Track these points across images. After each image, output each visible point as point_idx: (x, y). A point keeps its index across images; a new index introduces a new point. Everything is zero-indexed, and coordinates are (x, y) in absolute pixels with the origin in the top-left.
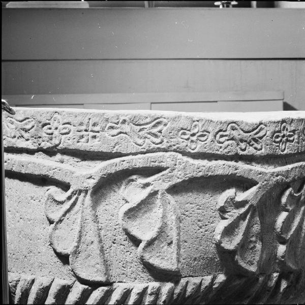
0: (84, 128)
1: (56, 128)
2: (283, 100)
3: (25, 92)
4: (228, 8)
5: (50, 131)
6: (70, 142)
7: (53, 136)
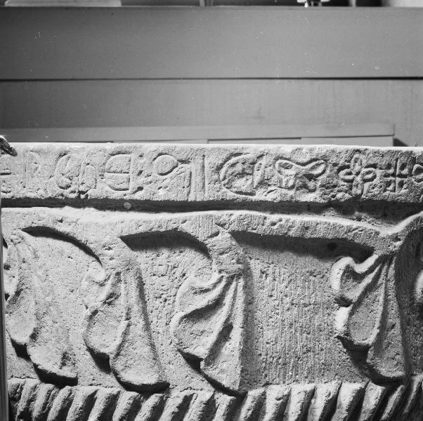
0: (391, 171)
1: (358, 174)
2: (393, 135)
3: (36, 124)
5: (350, 177)
6: (376, 191)
7: (354, 183)
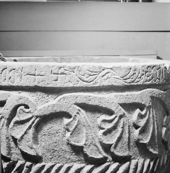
2: (157, 55)
4: (126, 2)
